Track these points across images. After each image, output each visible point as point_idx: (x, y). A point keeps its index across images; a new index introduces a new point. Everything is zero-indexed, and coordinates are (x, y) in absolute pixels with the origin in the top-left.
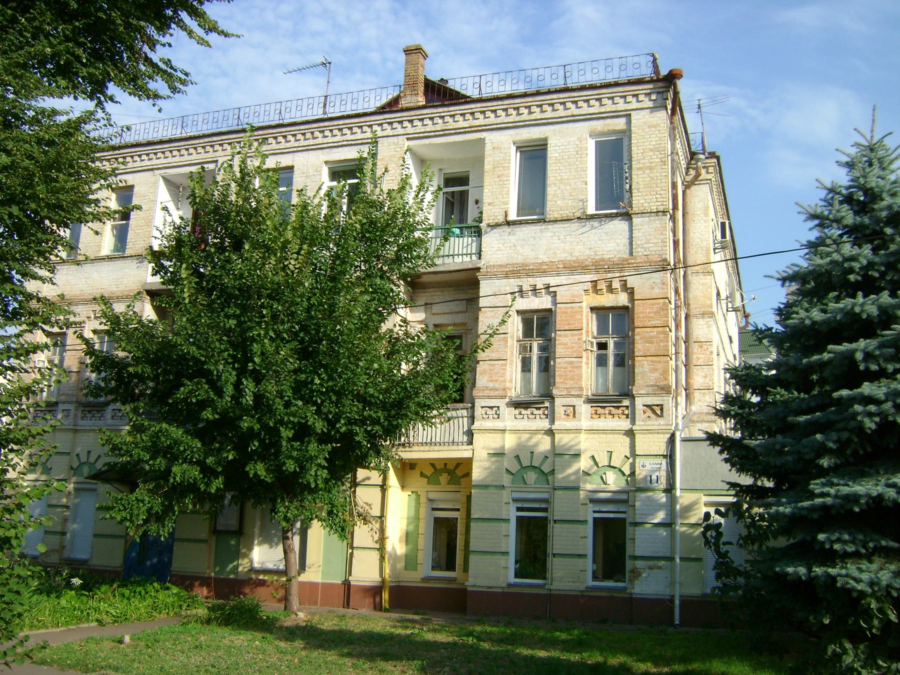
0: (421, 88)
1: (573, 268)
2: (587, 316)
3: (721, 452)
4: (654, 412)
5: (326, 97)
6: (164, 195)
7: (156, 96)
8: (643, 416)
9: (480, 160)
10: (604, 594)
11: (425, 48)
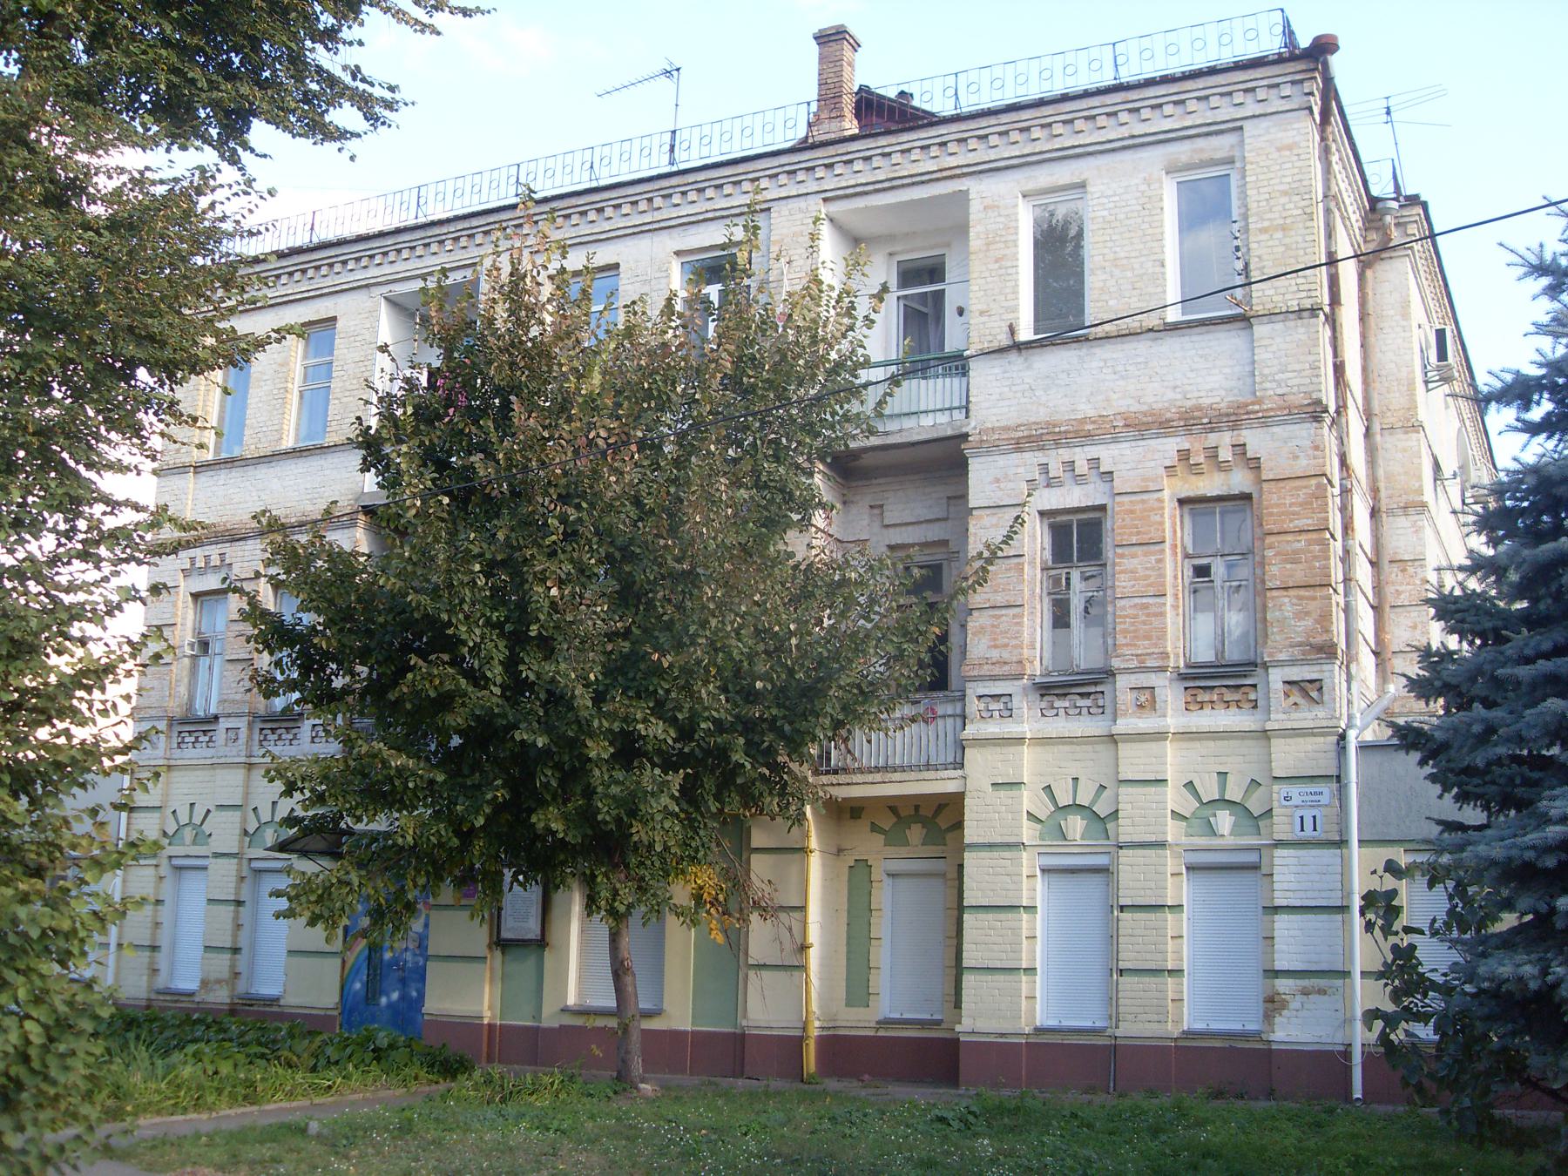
0: (848, 103)
1: (1145, 426)
2: (1173, 517)
3: (1423, 763)
4: (1306, 694)
5: (674, 132)
6: (386, 328)
7: (343, 135)
8: (1286, 704)
9: (962, 229)
10: (1218, 1044)
11: (852, 29)
